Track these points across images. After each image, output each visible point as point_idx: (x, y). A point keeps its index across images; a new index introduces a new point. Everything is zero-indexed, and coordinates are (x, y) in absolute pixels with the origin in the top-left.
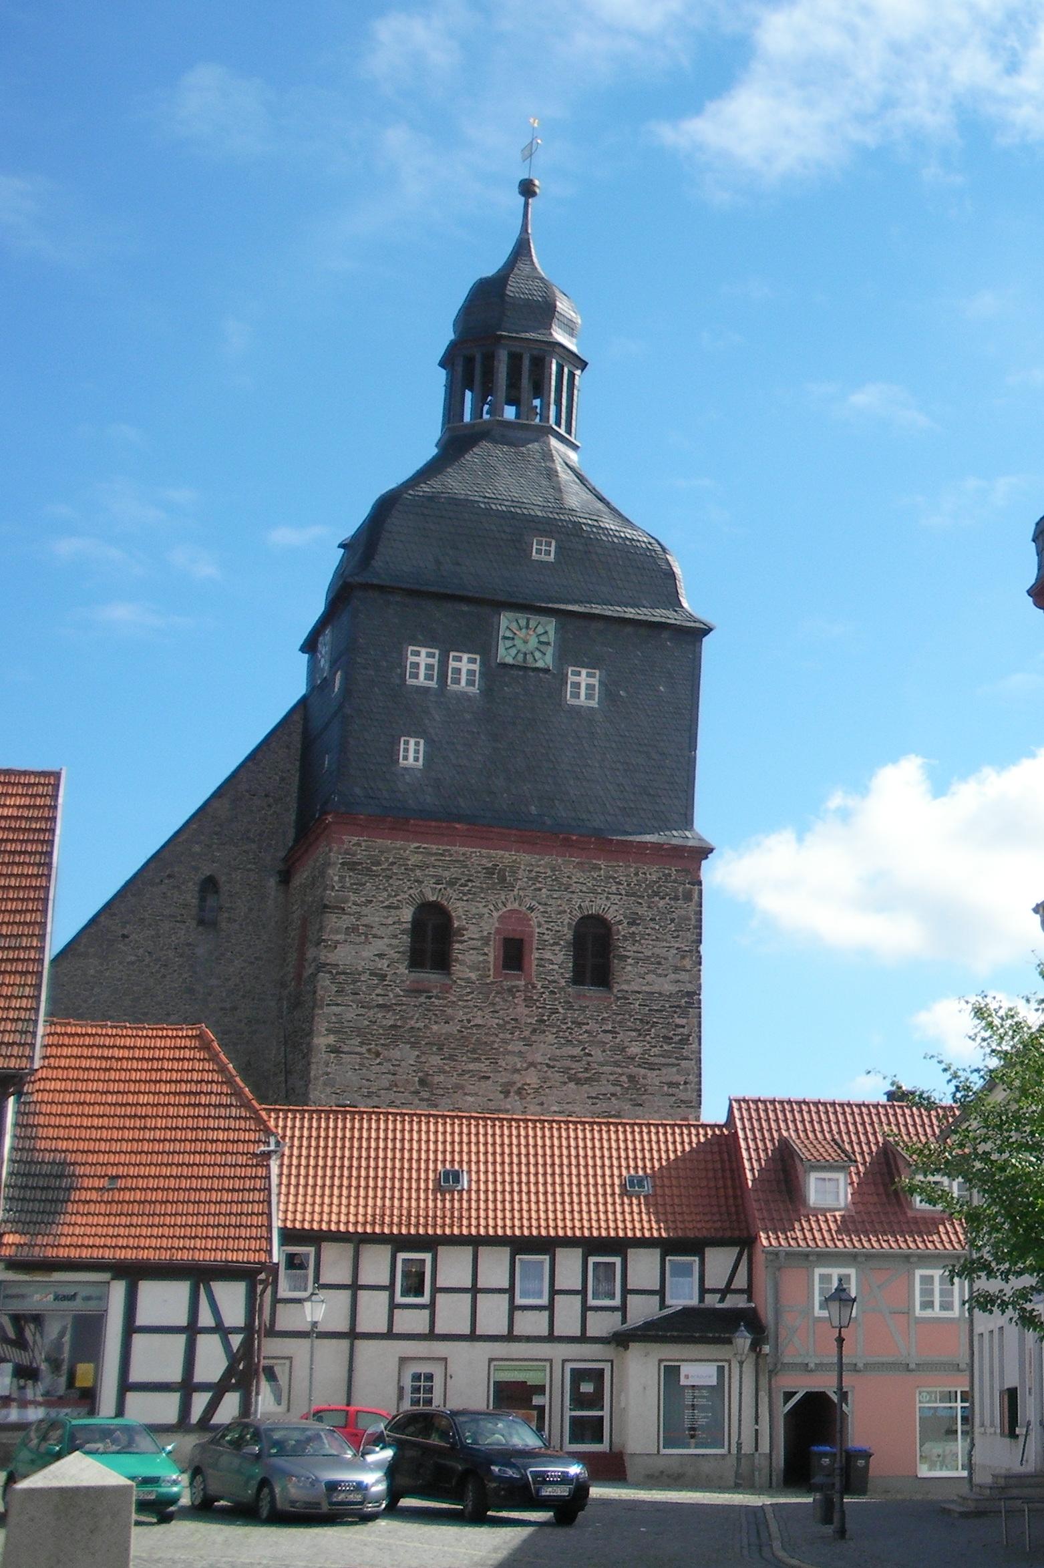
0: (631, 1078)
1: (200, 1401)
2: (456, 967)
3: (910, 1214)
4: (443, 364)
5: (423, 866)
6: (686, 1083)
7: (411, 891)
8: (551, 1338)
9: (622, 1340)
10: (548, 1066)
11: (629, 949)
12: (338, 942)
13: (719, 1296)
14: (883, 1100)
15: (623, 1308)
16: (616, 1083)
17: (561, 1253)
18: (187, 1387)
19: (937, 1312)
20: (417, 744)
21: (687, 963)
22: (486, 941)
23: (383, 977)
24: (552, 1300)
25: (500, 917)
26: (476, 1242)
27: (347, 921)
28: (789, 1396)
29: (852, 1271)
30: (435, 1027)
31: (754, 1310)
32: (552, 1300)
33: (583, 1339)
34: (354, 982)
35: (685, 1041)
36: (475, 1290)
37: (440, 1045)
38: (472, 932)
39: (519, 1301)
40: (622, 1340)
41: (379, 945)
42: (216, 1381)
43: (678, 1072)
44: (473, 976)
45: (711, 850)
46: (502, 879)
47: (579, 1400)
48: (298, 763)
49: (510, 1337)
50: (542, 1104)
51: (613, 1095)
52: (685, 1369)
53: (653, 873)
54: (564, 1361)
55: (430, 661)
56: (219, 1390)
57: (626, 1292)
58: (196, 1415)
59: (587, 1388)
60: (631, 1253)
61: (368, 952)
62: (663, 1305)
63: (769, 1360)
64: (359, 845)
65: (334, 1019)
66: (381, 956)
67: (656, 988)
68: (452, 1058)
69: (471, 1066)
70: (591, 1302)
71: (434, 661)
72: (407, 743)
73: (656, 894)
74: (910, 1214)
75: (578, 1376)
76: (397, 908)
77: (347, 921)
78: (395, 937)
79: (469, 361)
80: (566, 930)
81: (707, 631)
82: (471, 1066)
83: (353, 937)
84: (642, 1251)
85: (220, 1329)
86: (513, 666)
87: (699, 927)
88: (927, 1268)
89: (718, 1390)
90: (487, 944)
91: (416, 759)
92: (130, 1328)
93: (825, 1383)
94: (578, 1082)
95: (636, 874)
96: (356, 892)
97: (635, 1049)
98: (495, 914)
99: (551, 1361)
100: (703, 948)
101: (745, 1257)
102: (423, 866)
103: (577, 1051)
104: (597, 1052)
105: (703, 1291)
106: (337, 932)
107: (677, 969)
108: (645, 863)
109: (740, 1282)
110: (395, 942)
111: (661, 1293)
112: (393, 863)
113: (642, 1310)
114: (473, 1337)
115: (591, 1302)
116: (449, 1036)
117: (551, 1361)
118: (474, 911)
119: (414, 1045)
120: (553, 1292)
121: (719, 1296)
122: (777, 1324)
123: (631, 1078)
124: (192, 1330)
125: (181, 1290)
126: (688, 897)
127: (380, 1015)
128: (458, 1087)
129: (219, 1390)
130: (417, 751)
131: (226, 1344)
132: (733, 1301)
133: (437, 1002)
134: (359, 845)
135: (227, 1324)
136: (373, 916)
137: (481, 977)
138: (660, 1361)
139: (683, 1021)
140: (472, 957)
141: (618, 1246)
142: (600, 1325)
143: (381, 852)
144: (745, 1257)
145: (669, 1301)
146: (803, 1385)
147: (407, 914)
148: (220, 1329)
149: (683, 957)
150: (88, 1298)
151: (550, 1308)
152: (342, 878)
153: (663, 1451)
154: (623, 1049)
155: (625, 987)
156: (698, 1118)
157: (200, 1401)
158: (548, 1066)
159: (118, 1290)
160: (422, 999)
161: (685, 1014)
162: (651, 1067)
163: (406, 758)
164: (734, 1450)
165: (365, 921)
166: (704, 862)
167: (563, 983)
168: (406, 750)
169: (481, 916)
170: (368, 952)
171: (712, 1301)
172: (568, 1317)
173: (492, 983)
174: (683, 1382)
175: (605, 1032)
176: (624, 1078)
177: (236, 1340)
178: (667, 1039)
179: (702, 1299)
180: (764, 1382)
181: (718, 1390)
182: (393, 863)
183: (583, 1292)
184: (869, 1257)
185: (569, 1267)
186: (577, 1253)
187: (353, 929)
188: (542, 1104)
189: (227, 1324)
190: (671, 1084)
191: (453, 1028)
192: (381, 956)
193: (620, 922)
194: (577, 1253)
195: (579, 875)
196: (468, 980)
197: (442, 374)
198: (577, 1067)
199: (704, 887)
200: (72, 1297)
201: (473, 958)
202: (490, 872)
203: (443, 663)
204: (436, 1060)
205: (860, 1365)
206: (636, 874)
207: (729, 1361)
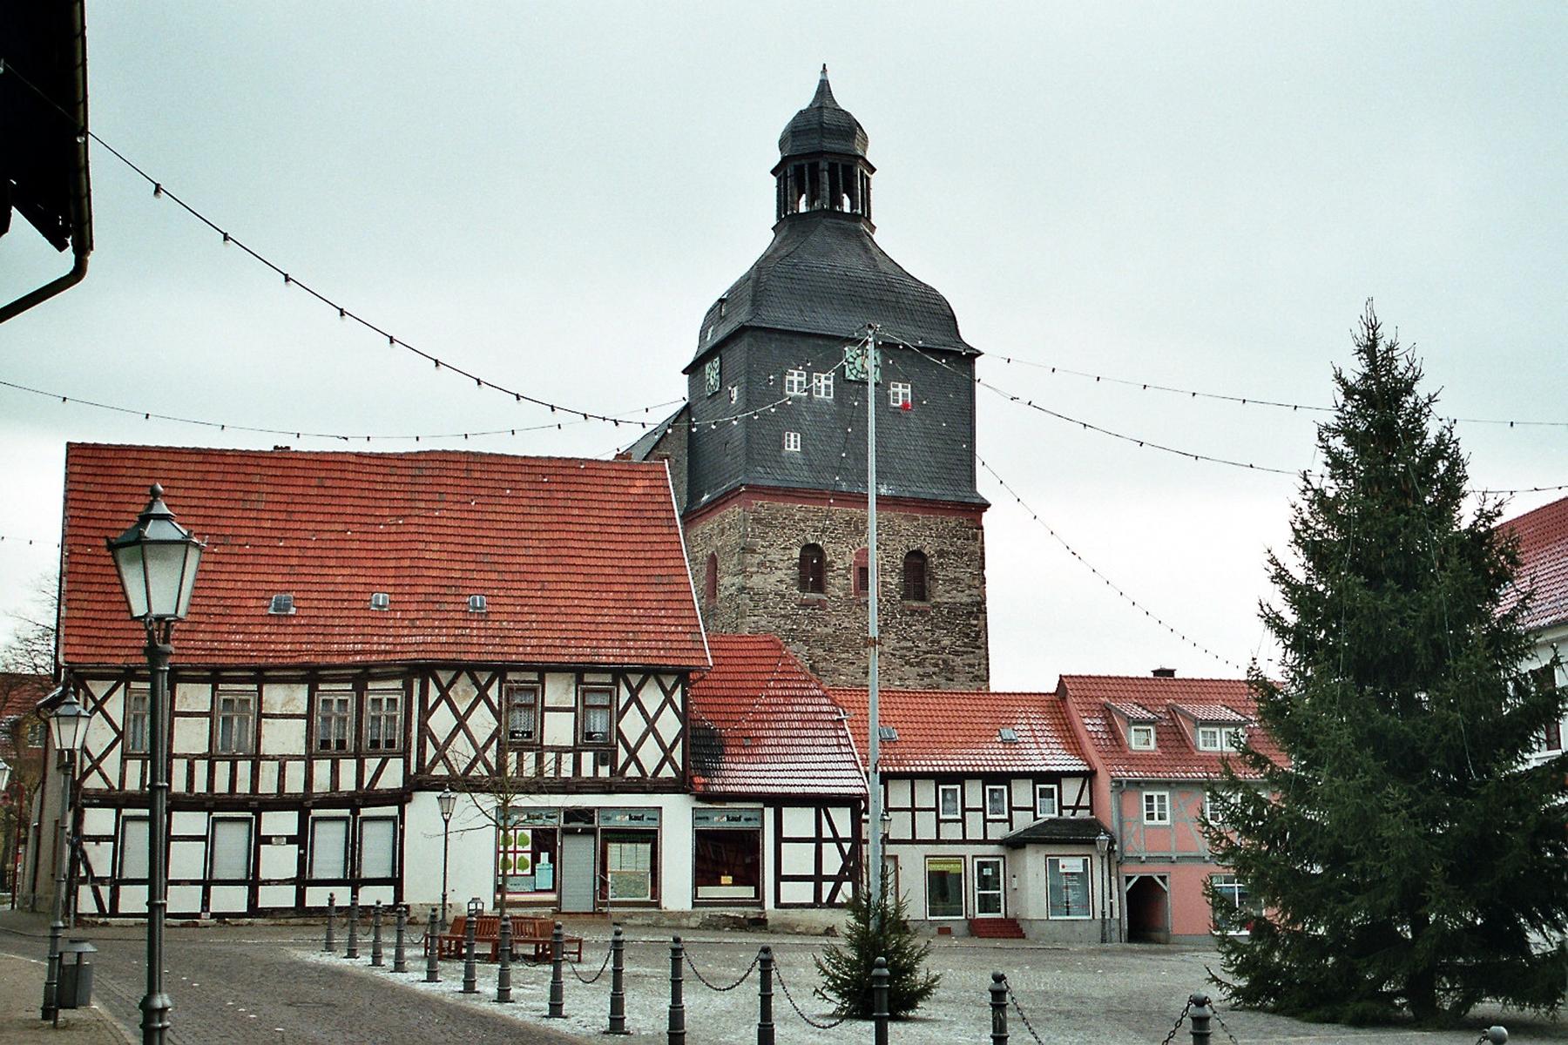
0: (945, 661)
1: (827, 887)
2: (830, 588)
3: (1197, 754)
4: (774, 172)
5: (804, 520)
6: (979, 665)
7: (799, 538)
8: (964, 841)
9: (1015, 844)
10: (892, 654)
11: (941, 574)
12: (752, 573)
13: (1071, 811)
14: (1151, 675)
15: (1010, 820)
16: (936, 665)
17: (968, 784)
18: (818, 878)
19: (1156, 821)
20: (796, 436)
21: (977, 583)
22: (848, 570)
23: (783, 596)
24: (963, 815)
25: (856, 554)
26: (913, 777)
27: (757, 558)
28: (1129, 879)
29: (1167, 794)
30: (818, 630)
31: (1096, 819)
32: (963, 815)
33: (985, 841)
34: (765, 600)
35: (978, 634)
36: (913, 810)
37: (821, 641)
38: (839, 564)
39: (941, 817)
40: (1015, 844)
41: (780, 574)
42: (836, 874)
43: (975, 658)
44: (841, 594)
45: (989, 505)
46: (857, 528)
47: (984, 882)
48: (686, 451)
49: (938, 841)
50: (889, 680)
51: (934, 673)
52: (1062, 861)
53: (952, 522)
54: (974, 857)
55: (800, 379)
56: (838, 880)
57: (1011, 809)
58: (825, 899)
59: (988, 872)
60: (1014, 783)
61: (773, 579)
62: (1036, 818)
63: (1117, 854)
64: (762, 506)
65: (753, 625)
66: (781, 581)
67: (958, 600)
68: (830, 650)
69: (843, 656)
70: (989, 816)
71: (803, 379)
72: (789, 435)
73: (955, 536)
74: (1197, 754)
75: (982, 866)
76: (790, 549)
77: (757, 558)
78: (790, 569)
79: (799, 171)
80: (898, 561)
81: (980, 354)
82: (843, 656)
83: (763, 570)
84: (1069, 779)
85: (836, 839)
86: (855, 381)
87: (983, 558)
88: (1161, 790)
89: (1083, 877)
90: (850, 573)
91: (796, 447)
92: (779, 839)
93: (1153, 871)
94: (911, 665)
95: (942, 523)
96: (763, 538)
97: (946, 642)
98: (853, 551)
99: (964, 857)
100: (985, 572)
101: (1087, 785)
102: (804, 520)
103: (911, 644)
104: (922, 645)
105: (1061, 807)
106: (752, 565)
107: (970, 587)
108: (948, 515)
109: (1085, 801)
110: (790, 572)
111: (1034, 809)
112: (785, 519)
113: (1023, 821)
114: (914, 841)
115: (989, 816)
116: (828, 635)
117: (964, 857)
118: (840, 550)
119: (806, 643)
120: (964, 810)
121: (1071, 811)
122: (1121, 830)
123: (945, 661)
124: (818, 840)
125: (810, 812)
126: (975, 537)
127: (782, 622)
128: (835, 671)
129: (838, 880)
130: (796, 441)
131: (841, 850)
132: (1081, 814)
133: (819, 612)
134: (762, 506)
135: (840, 836)
136: (774, 555)
137: (846, 595)
138: (1047, 856)
139: (975, 622)
140: (840, 581)
141: (1056, 777)
142: (998, 831)
143: (778, 511)
144: (1087, 785)
145: (1039, 815)
146: (1137, 872)
147: (796, 553)
148: (836, 839)
149: (974, 579)
150: (747, 820)
151: (963, 821)
152: (753, 530)
153: (929, 918)
154: (939, 642)
155: (938, 600)
156: (988, 688)
157: (827, 887)
158: (892, 654)
159: (769, 813)
160: (809, 611)
161: (977, 618)
162: (956, 653)
163: (789, 446)
164: (1098, 916)
165: (769, 558)
166: (984, 514)
167: (898, 597)
168: (789, 441)
169: (845, 553)
170: (773, 579)
171: (1067, 814)
172: (975, 829)
173: (854, 599)
174: (1061, 870)
175: (927, 630)
176: (940, 662)
177: (847, 847)
178: (968, 636)
179: (1060, 814)
180: (1114, 871)
181: (1083, 877)
182: (785, 519)
183: (983, 810)
184: (1179, 784)
185: (974, 794)
186: (979, 783)
187: (761, 564)
188: (889, 680)
189: (840, 836)
190: (970, 665)
191: (830, 630)
192: (781, 581)
193: (933, 556)
194: (979, 783)
195: (905, 525)
196: (838, 597)
197: (774, 180)
198: (911, 655)
199: (985, 531)
200: (739, 819)
201: (841, 582)
202: (848, 523)
203: (809, 381)
204: (820, 652)
205: (1174, 858)
206: (942, 523)
207: (1090, 856)
